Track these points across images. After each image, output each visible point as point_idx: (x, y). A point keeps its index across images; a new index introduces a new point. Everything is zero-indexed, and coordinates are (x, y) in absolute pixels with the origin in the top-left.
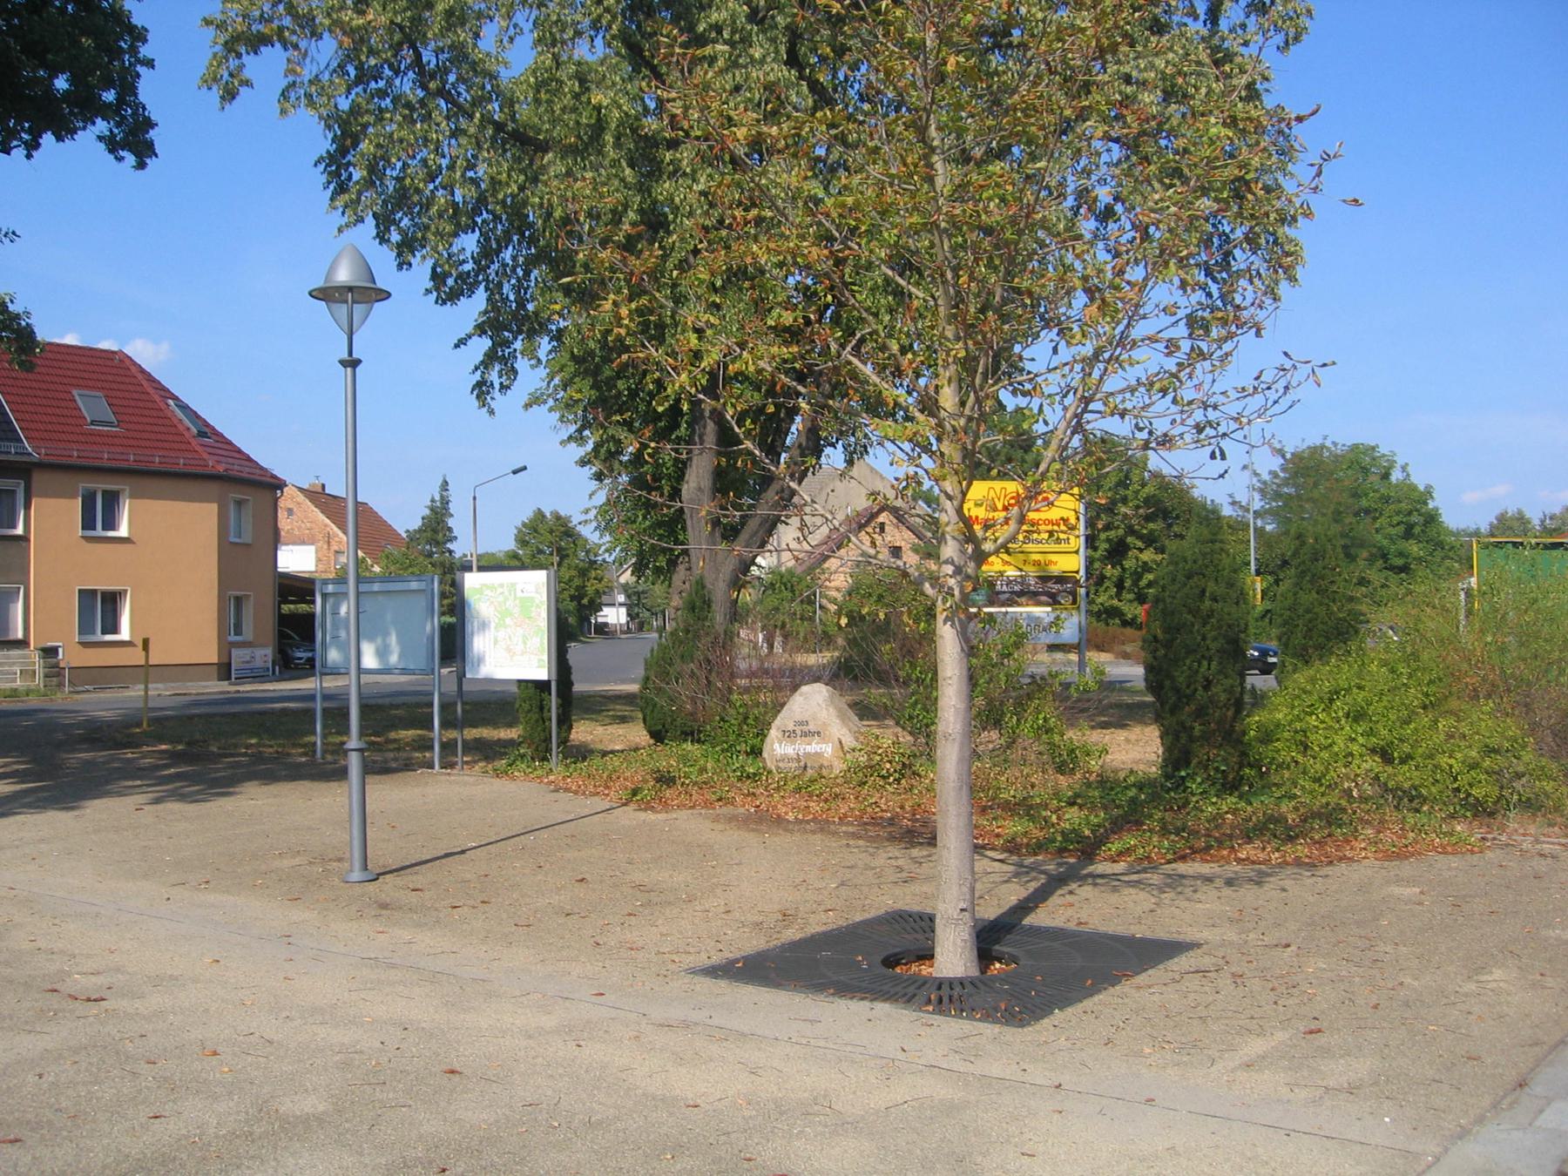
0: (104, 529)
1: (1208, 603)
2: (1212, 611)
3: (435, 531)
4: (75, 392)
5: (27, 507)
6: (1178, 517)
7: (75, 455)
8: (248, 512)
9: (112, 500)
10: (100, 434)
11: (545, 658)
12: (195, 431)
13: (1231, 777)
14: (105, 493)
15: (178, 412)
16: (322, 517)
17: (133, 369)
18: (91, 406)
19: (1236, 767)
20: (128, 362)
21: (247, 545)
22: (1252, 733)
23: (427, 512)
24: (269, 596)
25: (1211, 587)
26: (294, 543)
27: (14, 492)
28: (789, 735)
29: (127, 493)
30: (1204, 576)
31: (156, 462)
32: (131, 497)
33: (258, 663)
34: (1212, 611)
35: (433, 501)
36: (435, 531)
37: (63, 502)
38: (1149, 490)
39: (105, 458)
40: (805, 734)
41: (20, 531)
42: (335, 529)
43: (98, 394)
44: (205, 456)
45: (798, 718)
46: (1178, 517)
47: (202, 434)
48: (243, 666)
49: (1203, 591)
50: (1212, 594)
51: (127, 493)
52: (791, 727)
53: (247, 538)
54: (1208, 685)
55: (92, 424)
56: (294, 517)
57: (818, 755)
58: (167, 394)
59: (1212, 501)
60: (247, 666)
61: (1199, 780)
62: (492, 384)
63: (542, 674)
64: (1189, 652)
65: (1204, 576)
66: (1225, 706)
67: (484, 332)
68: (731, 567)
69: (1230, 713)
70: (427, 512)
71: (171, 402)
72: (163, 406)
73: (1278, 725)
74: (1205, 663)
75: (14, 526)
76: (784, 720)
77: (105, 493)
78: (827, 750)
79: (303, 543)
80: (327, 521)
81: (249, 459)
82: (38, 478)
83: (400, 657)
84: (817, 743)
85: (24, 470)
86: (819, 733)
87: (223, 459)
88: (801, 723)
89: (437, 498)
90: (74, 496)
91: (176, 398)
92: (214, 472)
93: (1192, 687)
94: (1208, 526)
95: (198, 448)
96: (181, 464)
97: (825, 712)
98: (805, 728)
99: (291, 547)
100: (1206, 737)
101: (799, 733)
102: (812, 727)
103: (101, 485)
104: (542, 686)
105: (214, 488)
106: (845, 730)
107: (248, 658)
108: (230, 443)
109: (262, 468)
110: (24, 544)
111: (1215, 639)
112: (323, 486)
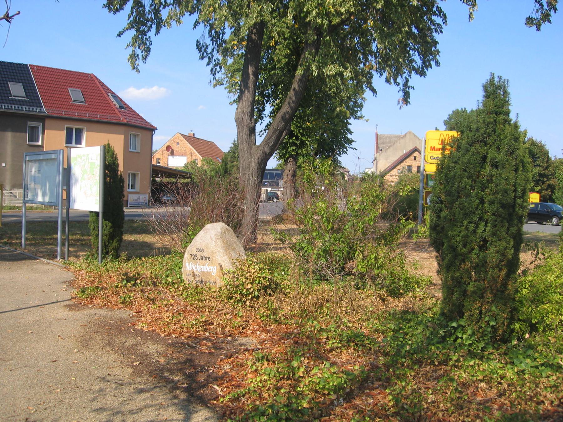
0: (76, 144)
1: (488, 168)
2: (492, 176)
3: (234, 153)
4: (69, 89)
5: (43, 133)
6: (539, 157)
7: (63, 114)
8: (139, 140)
9: (79, 133)
10: (77, 106)
11: (98, 198)
12: (118, 106)
13: (500, 332)
14: (76, 129)
15: (112, 99)
16: (190, 146)
17: (96, 81)
18: (75, 95)
19: (506, 322)
20: (94, 78)
21: (138, 153)
22: (525, 291)
23: (232, 145)
24: (148, 173)
25: (492, 153)
26: (179, 156)
27: (38, 127)
28: (194, 257)
29: (85, 129)
30: (486, 144)
31: (98, 117)
32: (87, 131)
33: (142, 201)
34: (492, 176)
35: (234, 141)
36: (234, 153)
37: (62, 132)
38: (527, 145)
39: (76, 115)
40: (202, 258)
41: (40, 143)
42: (194, 150)
43: (78, 90)
44: (120, 116)
45: (199, 246)
46: (539, 157)
47: (121, 107)
48: (134, 202)
49: (485, 157)
50: (492, 160)
51: (85, 129)
52: (195, 253)
53: (138, 150)
54: (484, 246)
55: (74, 101)
56: (179, 146)
57: (209, 273)
58: (108, 90)
59: (500, 77)
60: (136, 202)
61: (470, 332)
62: (138, 55)
63: (97, 210)
64: (466, 215)
65: (486, 144)
66: (497, 266)
67: (133, 27)
68: (258, 155)
69: (503, 273)
70: (232, 145)
71: (109, 94)
72: (106, 95)
73: (549, 287)
74: (482, 224)
75: (38, 141)
76: (191, 248)
77: (76, 129)
78: (214, 270)
79: (182, 155)
80: (192, 147)
81: (142, 118)
82: (47, 122)
83: (50, 198)
84: (209, 265)
85: (42, 119)
86: (209, 258)
87: (127, 117)
88: (201, 250)
89: (236, 140)
90: (63, 130)
91: (113, 94)
92: (122, 122)
93: (468, 247)
94: (494, 100)
95: (118, 113)
96: (109, 119)
97: (214, 243)
98: (202, 254)
99: (177, 157)
100: (480, 294)
101: (198, 256)
102: (205, 254)
103: (74, 126)
104: (97, 214)
105: (122, 129)
106: (226, 258)
107: (136, 198)
108: (135, 112)
109: (147, 122)
110: (41, 149)
111: (492, 203)
112: (194, 134)
